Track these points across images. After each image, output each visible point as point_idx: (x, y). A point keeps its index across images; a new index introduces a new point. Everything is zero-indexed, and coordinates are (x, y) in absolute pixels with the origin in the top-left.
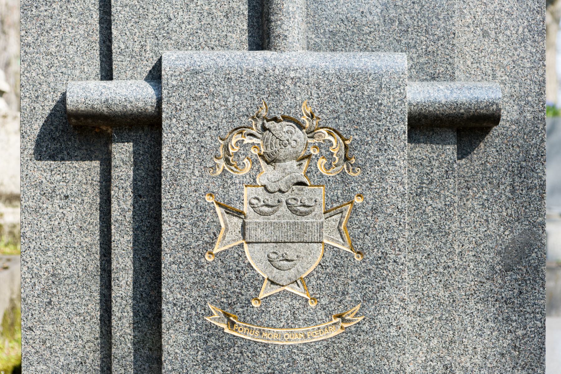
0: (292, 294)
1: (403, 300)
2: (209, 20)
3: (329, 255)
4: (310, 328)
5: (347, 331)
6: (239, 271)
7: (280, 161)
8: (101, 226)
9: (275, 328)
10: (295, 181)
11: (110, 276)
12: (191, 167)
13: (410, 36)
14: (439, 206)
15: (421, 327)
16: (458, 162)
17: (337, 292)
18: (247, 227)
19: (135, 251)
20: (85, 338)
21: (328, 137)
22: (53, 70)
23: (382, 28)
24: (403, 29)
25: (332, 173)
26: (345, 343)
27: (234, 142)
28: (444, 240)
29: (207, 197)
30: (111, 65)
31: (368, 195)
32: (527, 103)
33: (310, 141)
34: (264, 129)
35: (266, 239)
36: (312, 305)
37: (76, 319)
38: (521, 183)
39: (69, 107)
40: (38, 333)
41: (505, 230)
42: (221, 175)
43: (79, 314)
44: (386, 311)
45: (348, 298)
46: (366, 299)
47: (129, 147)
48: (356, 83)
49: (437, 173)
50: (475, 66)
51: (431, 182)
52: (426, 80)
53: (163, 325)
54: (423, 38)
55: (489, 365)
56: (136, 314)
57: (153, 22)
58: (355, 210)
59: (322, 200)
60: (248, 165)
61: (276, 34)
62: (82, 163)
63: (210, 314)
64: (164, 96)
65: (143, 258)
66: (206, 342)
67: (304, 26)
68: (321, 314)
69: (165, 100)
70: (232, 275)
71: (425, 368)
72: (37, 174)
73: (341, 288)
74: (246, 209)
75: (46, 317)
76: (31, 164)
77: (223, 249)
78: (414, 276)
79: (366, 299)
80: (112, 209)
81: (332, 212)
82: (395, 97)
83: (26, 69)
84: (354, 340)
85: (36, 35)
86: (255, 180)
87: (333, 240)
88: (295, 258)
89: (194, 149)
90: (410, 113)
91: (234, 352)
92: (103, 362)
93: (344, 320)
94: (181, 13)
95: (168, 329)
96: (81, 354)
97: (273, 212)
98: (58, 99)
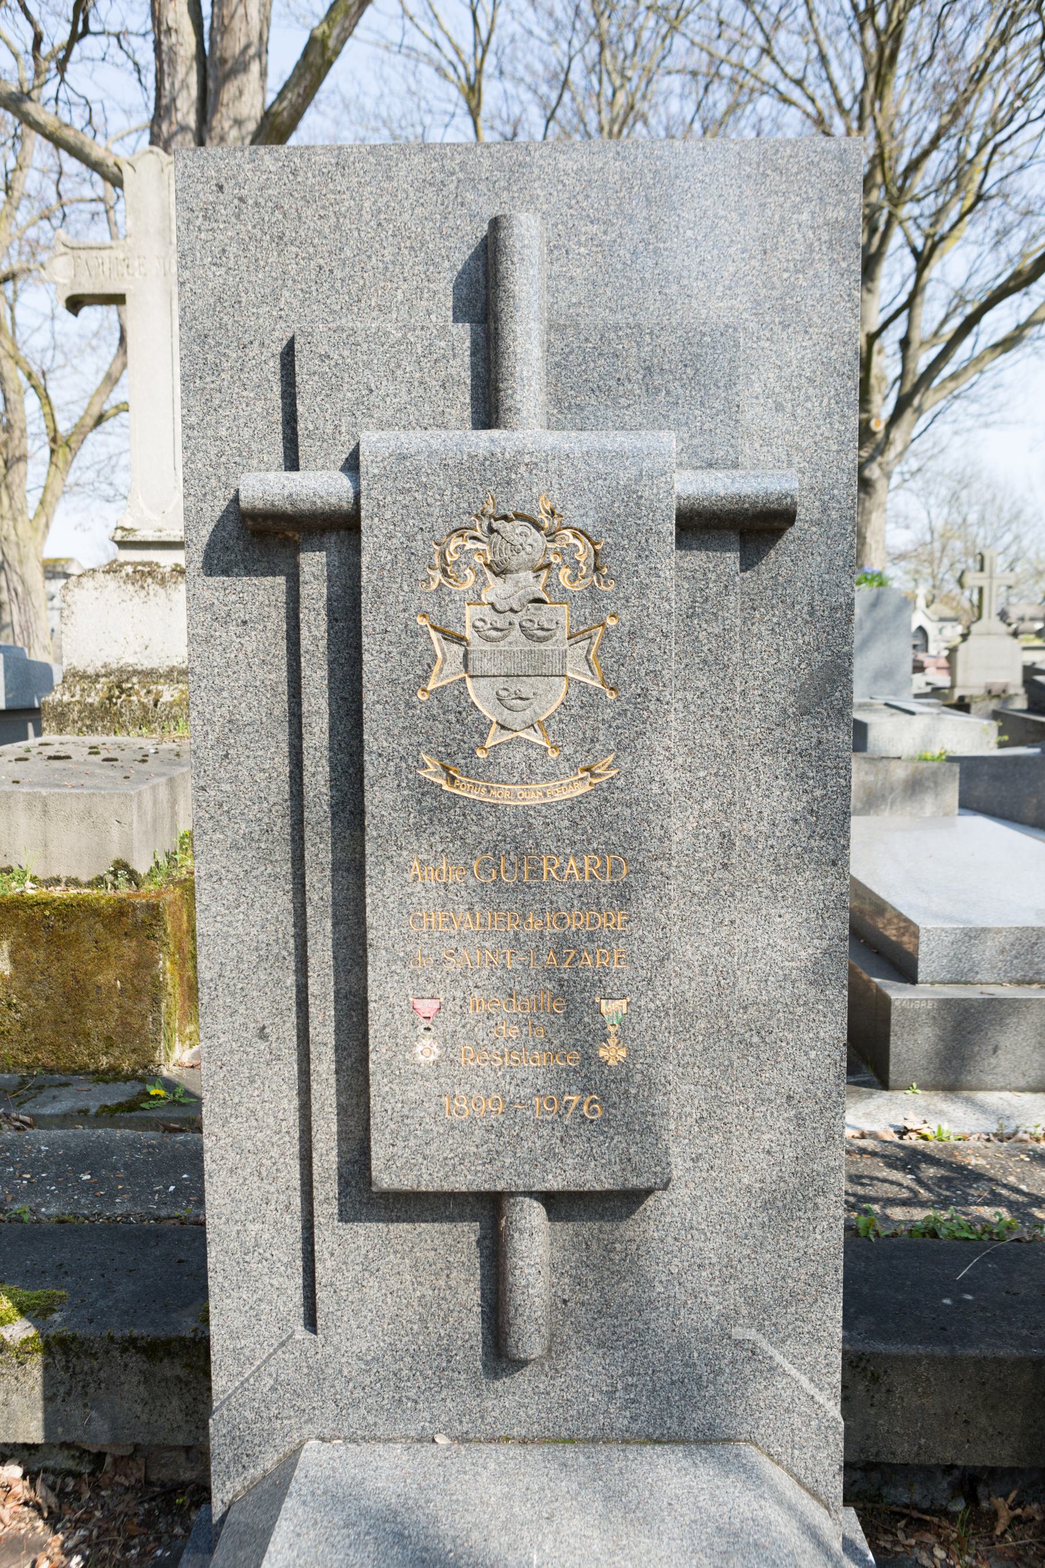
0: (527, 742)
1: (668, 749)
2: (421, 391)
3: (574, 692)
4: (550, 785)
5: (598, 788)
6: (460, 713)
7: (511, 572)
8: (289, 659)
9: (505, 783)
10: (531, 597)
11: (300, 722)
12: (399, 580)
13: (680, 410)
14: (716, 631)
15: (692, 785)
16: (741, 575)
17: (584, 739)
18: (470, 656)
19: (330, 689)
20: (272, 800)
21: (572, 540)
22: (223, 459)
23: (644, 400)
24: (672, 400)
25: (579, 586)
26: (595, 803)
27: (452, 547)
28: (721, 675)
29: (419, 619)
30: (296, 453)
31: (624, 615)
32: (832, 498)
33: (550, 545)
34: (491, 530)
35: (494, 672)
36: (553, 755)
37: (260, 776)
38: (823, 602)
39: (243, 505)
40: (213, 793)
41: (801, 662)
42: (436, 590)
43: (263, 770)
44: (647, 763)
45: (598, 746)
46: (621, 747)
47: (321, 557)
48: (609, 469)
49: (713, 589)
50: (765, 449)
51: (706, 600)
52: (701, 467)
53: (366, 781)
54: (698, 413)
55: (778, 834)
56: (333, 769)
57: (349, 394)
58: (607, 635)
59: (565, 621)
60: (471, 577)
61: (506, 406)
62: (263, 579)
63: (425, 766)
64: (363, 488)
65: (342, 698)
66: (419, 802)
67: (542, 398)
68: (564, 766)
69: (364, 494)
70: (452, 717)
71: (696, 836)
72: (207, 594)
73: (589, 733)
74: (469, 633)
75: (223, 774)
76: (199, 580)
77: (440, 684)
78: (684, 720)
79: (621, 747)
80: (302, 637)
81: (578, 638)
82: (659, 488)
83: (189, 458)
84: (606, 799)
85: (200, 414)
86: (479, 596)
87: (579, 673)
88: (531, 696)
89: (402, 557)
90: (678, 510)
91: (455, 814)
92: (293, 829)
93: (593, 775)
94: (384, 383)
95: (372, 786)
96: (266, 820)
97: (503, 638)
98: (231, 497)
